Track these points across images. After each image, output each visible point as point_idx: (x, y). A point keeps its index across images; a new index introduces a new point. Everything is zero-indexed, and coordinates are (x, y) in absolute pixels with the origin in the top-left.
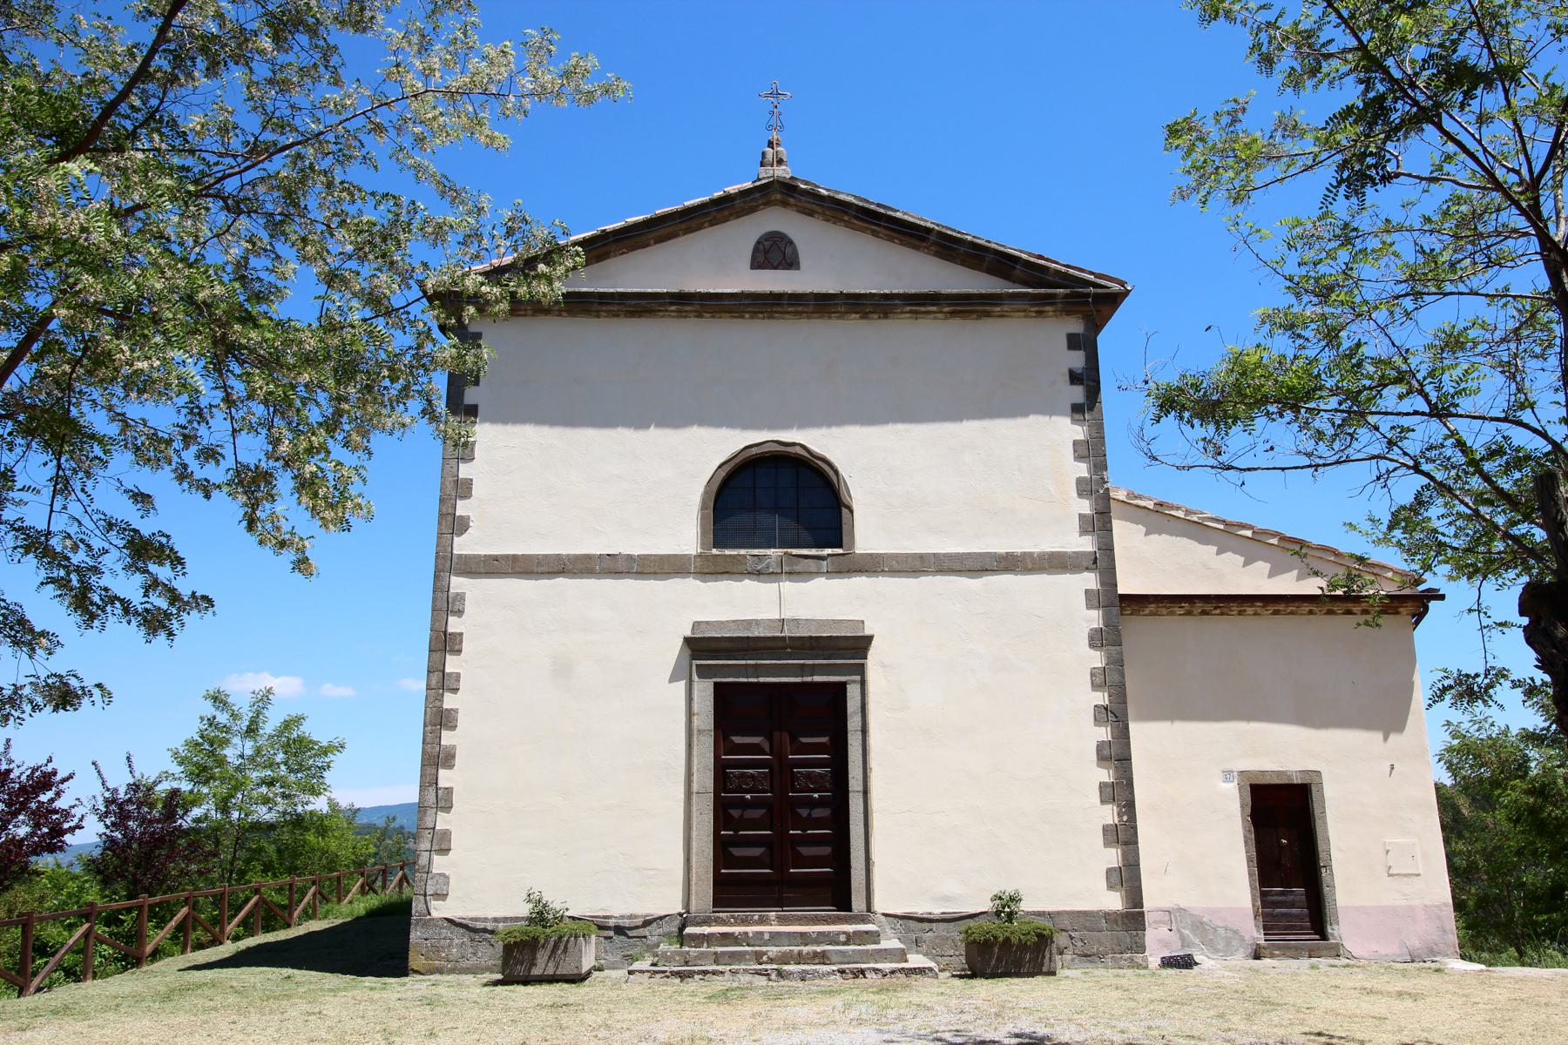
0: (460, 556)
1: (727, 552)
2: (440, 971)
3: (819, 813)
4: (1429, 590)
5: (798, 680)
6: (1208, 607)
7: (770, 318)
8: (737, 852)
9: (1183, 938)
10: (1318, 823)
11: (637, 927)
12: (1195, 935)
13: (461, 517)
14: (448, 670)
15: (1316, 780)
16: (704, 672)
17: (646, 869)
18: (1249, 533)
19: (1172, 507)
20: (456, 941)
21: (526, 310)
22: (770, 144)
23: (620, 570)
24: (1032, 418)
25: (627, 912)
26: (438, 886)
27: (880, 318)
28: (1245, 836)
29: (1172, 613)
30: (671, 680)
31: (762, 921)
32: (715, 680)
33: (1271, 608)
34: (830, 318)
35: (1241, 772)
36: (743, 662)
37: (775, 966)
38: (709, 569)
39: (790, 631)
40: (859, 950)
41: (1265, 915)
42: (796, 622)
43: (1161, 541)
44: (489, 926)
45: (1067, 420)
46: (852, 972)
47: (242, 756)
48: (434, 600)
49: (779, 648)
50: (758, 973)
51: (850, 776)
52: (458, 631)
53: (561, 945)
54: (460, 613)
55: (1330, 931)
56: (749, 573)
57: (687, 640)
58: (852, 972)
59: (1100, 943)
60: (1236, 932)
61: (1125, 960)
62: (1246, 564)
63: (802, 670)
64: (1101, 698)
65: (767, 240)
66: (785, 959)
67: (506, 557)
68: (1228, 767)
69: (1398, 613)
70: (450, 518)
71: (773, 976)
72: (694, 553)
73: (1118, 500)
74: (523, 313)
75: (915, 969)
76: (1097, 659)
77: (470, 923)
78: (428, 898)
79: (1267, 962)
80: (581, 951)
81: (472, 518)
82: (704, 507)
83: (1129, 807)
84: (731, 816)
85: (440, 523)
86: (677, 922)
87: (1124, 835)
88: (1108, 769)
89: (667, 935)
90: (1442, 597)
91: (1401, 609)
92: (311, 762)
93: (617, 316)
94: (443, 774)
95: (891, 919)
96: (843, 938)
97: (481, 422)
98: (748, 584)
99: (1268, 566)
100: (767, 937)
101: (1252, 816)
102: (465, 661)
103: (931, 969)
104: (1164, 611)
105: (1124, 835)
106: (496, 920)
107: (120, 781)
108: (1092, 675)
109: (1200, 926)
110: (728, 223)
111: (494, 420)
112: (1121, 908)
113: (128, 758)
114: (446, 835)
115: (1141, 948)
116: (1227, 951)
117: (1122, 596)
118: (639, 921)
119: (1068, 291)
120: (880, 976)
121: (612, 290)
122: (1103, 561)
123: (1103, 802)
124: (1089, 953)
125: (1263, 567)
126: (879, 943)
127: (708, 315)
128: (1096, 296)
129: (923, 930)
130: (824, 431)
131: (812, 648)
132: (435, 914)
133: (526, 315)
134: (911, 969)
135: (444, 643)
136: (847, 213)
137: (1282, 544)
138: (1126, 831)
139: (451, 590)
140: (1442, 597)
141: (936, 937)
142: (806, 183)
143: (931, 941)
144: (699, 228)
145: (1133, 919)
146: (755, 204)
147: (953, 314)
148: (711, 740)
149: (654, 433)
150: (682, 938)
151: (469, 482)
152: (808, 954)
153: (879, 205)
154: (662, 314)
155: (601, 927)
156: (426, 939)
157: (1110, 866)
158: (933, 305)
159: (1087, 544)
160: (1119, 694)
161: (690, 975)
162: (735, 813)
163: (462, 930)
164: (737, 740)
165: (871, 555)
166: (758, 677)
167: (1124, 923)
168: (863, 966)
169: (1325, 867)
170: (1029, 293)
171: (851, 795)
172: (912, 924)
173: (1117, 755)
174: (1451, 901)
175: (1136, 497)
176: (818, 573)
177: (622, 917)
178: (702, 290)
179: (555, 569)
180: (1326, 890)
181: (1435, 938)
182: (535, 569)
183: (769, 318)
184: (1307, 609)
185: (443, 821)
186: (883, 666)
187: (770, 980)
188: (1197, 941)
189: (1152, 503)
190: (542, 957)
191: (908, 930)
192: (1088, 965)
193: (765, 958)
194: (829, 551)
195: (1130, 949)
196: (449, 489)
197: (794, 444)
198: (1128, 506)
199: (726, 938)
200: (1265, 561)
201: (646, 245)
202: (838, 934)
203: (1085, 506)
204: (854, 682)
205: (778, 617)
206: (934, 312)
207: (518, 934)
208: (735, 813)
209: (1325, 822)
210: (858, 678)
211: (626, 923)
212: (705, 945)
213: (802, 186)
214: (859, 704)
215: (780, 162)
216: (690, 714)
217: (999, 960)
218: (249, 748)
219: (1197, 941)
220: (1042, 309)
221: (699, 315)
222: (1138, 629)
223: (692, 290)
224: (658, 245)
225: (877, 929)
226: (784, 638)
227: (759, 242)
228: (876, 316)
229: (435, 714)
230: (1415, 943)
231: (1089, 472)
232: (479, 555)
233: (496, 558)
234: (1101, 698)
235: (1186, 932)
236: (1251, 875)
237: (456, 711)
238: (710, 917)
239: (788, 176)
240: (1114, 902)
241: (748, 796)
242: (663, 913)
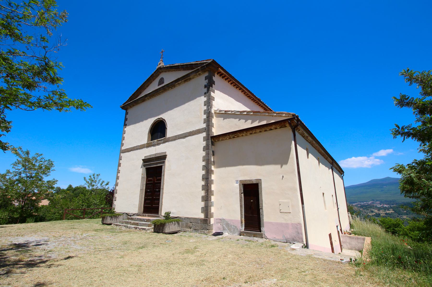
9: (223, 227)
12: (226, 227)
18: (245, 113)
27: (174, 88)
31: (146, 216)
36: (150, 163)
38: (148, 146)
43: (227, 120)
55: (261, 229)
59: (198, 227)
60: (236, 227)
61: (203, 232)
68: (237, 180)
73: (217, 113)
77: (128, 214)
87: (207, 199)
88: (204, 181)
99: (251, 121)
105: (207, 199)
109: (228, 225)
110: (156, 79)
116: (234, 233)
119: (200, 67)
124: (196, 229)
125: (250, 121)
127: (152, 98)
135: (119, 165)
137: (254, 114)
138: (206, 197)
144: (152, 82)
147: (185, 81)
149: (144, 121)
166: (151, 166)
167: (203, 222)
169: (261, 209)
170: (193, 71)
176: (161, 143)
180: (261, 216)
181: (295, 235)
183: (159, 94)
188: (227, 229)
189: (224, 111)
198: (219, 114)
200: (250, 120)
201: (146, 89)
206: (181, 83)
209: (262, 195)
213: (162, 67)
219: (227, 229)
223: (146, 94)
224: (148, 88)
230: (288, 236)
240: (202, 216)
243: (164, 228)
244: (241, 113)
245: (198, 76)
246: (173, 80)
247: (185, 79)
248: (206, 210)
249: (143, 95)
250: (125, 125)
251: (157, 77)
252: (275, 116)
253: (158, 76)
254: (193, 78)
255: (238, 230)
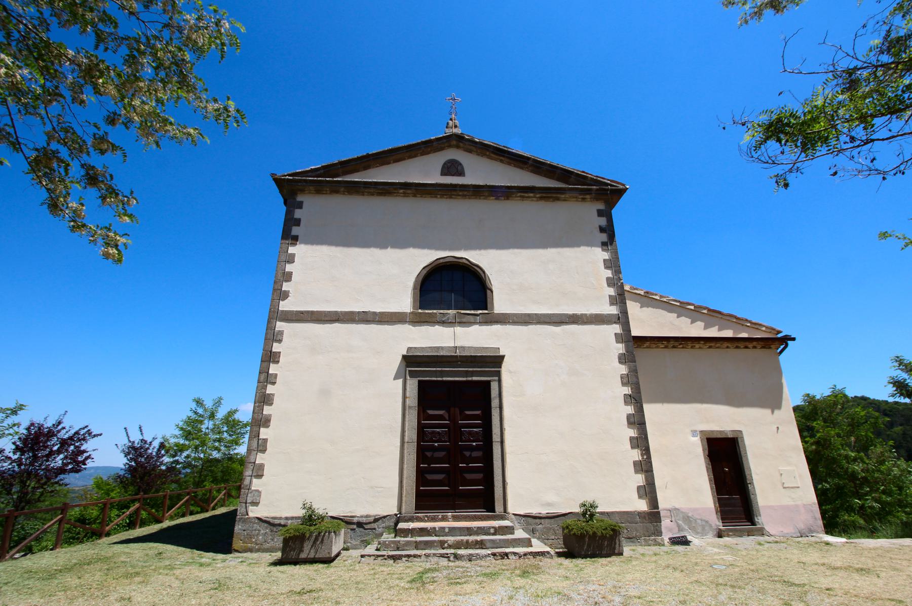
0: (283, 311)
1: (427, 311)
2: (251, 550)
3: (476, 454)
4: (786, 336)
5: (464, 379)
6: (676, 344)
7: (451, 198)
8: (430, 477)
9: (679, 526)
10: (744, 459)
11: (370, 523)
12: (685, 524)
13: (285, 291)
14: (270, 372)
15: (740, 436)
16: (413, 374)
17: (376, 487)
19: (653, 294)
20: (262, 532)
21: (326, 191)
22: (451, 119)
23: (369, 319)
24: (582, 248)
25: (365, 513)
26: (254, 498)
27: (505, 199)
28: (706, 467)
29: (657, 347)
30: (395, 379)
31: (444, 519)
32: (419, 379)
33: (708, 345)
34: (480, 199)
35: (701, 432)
36: (435, 369)
37: (452, 551)
38: (416, 320)
39: (460, 353)
40: (504, 540)
41: (721, 512)
42: (463, 348)
44: (283, 522)
45: (599, 249)
46: (500, 555)
47: (208, 428)
48: (266, 334)
49: (454, 362)
50: (442, 556)
51: (493, 433)
52: (278, 351)
53: (320, 538)
54: (280, 341)
55: (756, 520)
56: (438, 322)
57: (404, 357)
58: (500, 555)
59: (637, 531)
60: (707, 522)
62: (692, 323)
63: (467, 374)
64: (627, 390)
65: (449, 163)
66: (458, 546)
67: (308, 312)
69: (770, 348)
70: (279, 292)
71: (452, 558)
72: (409, 311)
74: (325, 192)
75: (538, 552)
76: (623, 369)
77: (271, 520)
78: (248, 505)
79: (726, 539)
80: (332, 542)
81: (291, 292)
82: (415, 288)
83: (646, 451)
84: (427, 456)
85: (273, 294)
86: (394, 520)
87: (645, 467)
89: (388, 528)
90: (794, 339)
91: (772, 346)
92: (239, 430)
93: (373, 195)
94: (263, 431)
95: (518, 517)
96: (492, 531)
97: (299, 243)
98: (438, 328)
99: (703, 324)
100: (447, 530)
101: (709, 456)
102: (281, 367)
103: (548, 553)
104: (654, 346)
105: (645, 467)
106: (287, 518)
107: (136, 438)
108: (621, 378)
109: (687, 519)
111: (307, 242)
112: (646, 510)
113: (140, 428)
114: (261, 467)
115: (659, 533)
116: (703, 533)
117: (633, 336)
118: (372, 519)
119: (598, 187)
120: (517, 557)
121: (370, 180)
122: (623, 319)
123: (632, 448)
125: (700, 324)
126: (513, 533)
127: (419, 196)
128: (612, 191)
129: (536, 524)
130: (478, 252)
131: (471, 362)
132: (251, 515)
133: (326, 194)
134: (536, 553)
135: (270, 357)
136: (488, 150)
139: (276, 329)
140: (794, 339)
141: (544, 528)
142: (468, 136)
143: (541, 531)
144: (415, 156)
145: (653, 516)
146: (443, 146)
147: (541, 198)
148: (416, 413)
149: (390, 251)
150: (397, 532)
151: (290, 274)
152: (472, 542)
153: (504, 146)
154: (395, 194)
155: (348, 523)
156: (244, 531)
157: (639, 485)
158: (532, 193)
159: (614, 310)
160: (636, 388)
161: (399, 557)
162: (429, 454)
163: (266, 525)
164: (431, 412)
165: (502, 314)
166: (442, 377)
167: (649, 518)
168: (507, 550)
171: (494, 443)
172: (530, 520)
173: (638, 421)
174: (816, 502)
175: (635, 289)
176: (475, 323)
177: (362, 517)
178: (416, 182)
179: (334, 318)
180: (752, 496)
182: (323, 319)
184: (726, 345)
185: (260, 459)
186: (510, 372)
187: (449, 560)
188: (686, 527)
189: (643, 292)
190: (307, 546)
191: (528, 524)
192: (631, 544)
193: (446, 545)
194: (481, 312)
195: (654, 534)
196: (280, 275)
197: (462, 258)
199: (423, 532)
201: (389, 163)
202: (490, 528)
203: (612, 291)
204: (495, 380)
205: (453, 345)
207: (292, 531)
208: (429, 454)
209: (747, 459)
210: (497, 378)
211: (364, 520)
212: (410, 535)
214: (497, 393)
215: (456, 127)
216: (404, 397)
217: (589, 546)
218: (211, 424)
220: (585, 197)
221: (415, 196)
222: (643, 355)
223: (411, 182)
225: (512, 525)
226: (457, 356)
227: (445, 164)
228: (503, 198)
229: (261, 396)
230: (801, 526)
231: (612, 274)
232: (293, 311)
233: (302, 312)
234: (627, 390)
235: (680, 522)
236: (712, 489)
237: (273, 395)
238: (413, 516)
239: (459, 133)
240: (642, 506)
241: (436, 444)
242: (385, 514)
243: (617, 541)
244: (682, 305)
245: (577, 201)
246: (516, 185)
247: (546, 194)
248: (649, 491)
249: (356, 178)
250: (289, 236)
251: (435, 152)
252: (748, 326)
253: (439, 151)
254: (564, 200)
255: (712, 526)
